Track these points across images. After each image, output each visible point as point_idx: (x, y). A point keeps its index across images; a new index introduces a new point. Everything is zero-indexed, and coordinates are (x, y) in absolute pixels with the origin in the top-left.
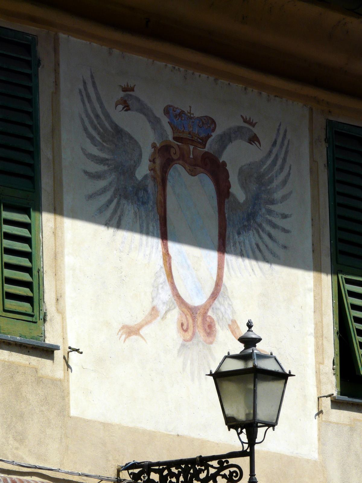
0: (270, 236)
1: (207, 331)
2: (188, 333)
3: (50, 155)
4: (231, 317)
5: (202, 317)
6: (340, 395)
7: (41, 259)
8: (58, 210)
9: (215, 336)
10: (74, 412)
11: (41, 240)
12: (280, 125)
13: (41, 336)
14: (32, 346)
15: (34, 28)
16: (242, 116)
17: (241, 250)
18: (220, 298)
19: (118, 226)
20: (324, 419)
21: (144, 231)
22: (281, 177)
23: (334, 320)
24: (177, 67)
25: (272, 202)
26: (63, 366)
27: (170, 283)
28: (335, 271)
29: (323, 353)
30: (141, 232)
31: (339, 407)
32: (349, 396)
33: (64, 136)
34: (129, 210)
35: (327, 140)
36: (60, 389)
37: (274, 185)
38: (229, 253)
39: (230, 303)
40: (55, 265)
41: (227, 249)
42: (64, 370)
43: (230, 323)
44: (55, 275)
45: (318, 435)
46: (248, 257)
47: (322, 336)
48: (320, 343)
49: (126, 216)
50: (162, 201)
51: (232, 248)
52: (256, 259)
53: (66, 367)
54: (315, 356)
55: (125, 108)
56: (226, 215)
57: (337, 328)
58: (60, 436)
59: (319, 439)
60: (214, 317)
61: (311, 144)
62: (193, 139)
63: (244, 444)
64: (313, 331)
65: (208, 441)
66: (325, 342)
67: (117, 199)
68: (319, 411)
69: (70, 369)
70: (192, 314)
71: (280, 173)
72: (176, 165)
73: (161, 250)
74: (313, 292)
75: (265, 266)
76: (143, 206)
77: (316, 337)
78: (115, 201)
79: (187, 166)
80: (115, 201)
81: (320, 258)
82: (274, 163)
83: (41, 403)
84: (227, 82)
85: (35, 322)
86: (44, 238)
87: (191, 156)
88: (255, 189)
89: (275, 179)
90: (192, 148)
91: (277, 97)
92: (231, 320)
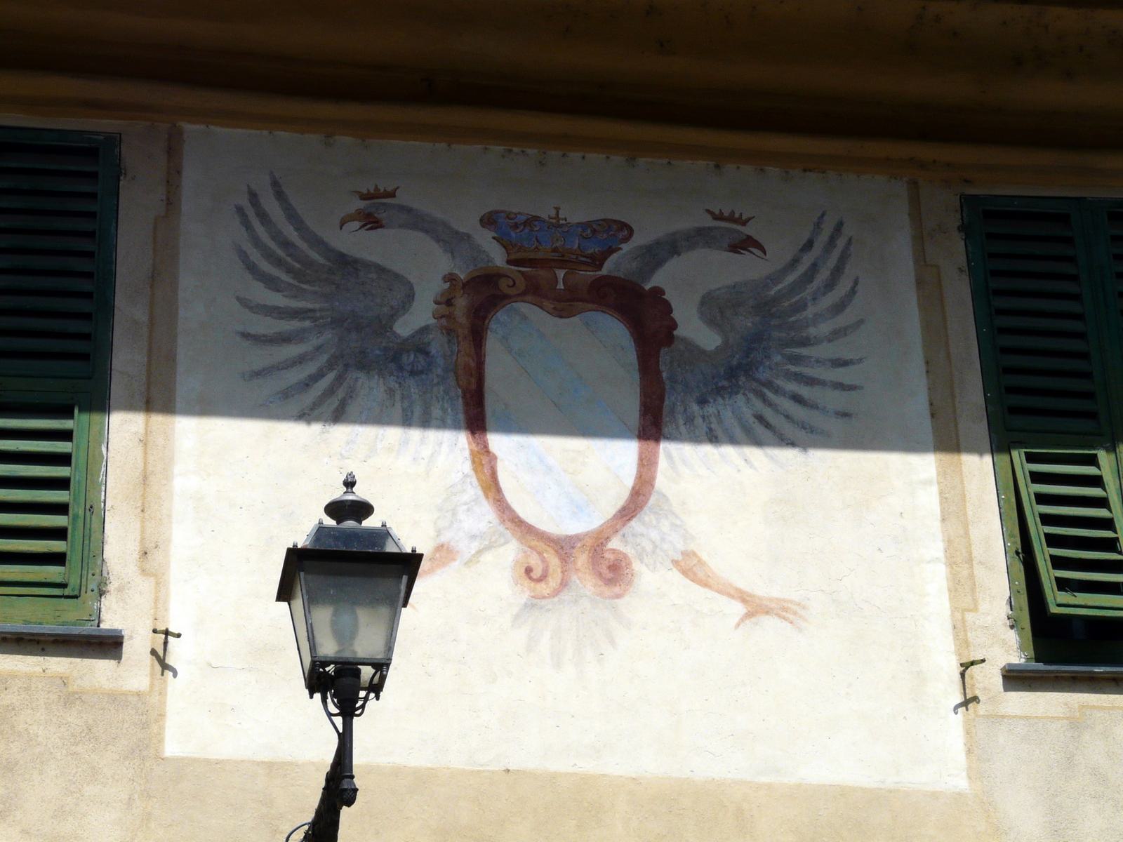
0: (797, 399)
1: (604, 576)
2: (547, 584)
3: (141, 315)
4: (680, 546)
5: (589, 553)
6: (1036, 662)
7: (1095, 672)
8: (158, 398)
9: (630, 583)
10: (173, 747)
11: (105, 456)
12: (823, 215)
13: (90, 620)
14: (52, 639)
15: (108, 121)
16: (708, 211)
17: (711, 430)
18: (646, 516)
19: (339, 416)
20: (982, 712)
21: (416, 416)
22: (828, 300)
23: (1004, 529)
24: (515, 149)
25: (805, 342)
26: (149, 668)
27: (491, 500)
28: (1000, 444)
29: (973, 590)
30: (407, 421)
31: (1030, 686)
32: (1046, 663)
33: (187, 282)
34: (372, 387)
35: (963, 228)
36: (146, 715)
37: (810, 312)
38: (670, 438)
39: (678, 522)
40: (143, 495)
41: (665, 430)
42: (152, 675)
43: (680, 558)
44: (142, 511)
45: (965, 745)
46: (733, 441)
47: (970, 560)
48: (965, 573)
49: (363, 398)
50: (473, 364)
51: (683, 429)
52: (758, 442)
53: (158, 668)
54: (950, 599)
55: (369, 226)
56: (664, 375)
57: (1014, 543)
58: (127, 797)
59: (969, 752)
60: (629, 551)
61: (919, 240)
62: (565, 258)
63: (332, 717)
64: (941, 554)
65: (604, 775)
66: (979, 571)
67: (335, 372)
68: (968, 698)
69: (172, 671)
70: (560, 551)
71: (824, 294)
72: (513, 304)
73: (466, 446)
74: (937, 486)
75: (789, 455)
76: (414, 378)
77: (951, 563)
78: (331, 376)
79: (546, 304)
80: (331, 376)
81: (956, 426)
82: (809, 276)
83: (72, 740)
84: (665, 161)
85: (76, 597)
86: (112, 451)
87: (561, 286)
88: (749, 324)
89: (809, 304)
90: (561, 274)
91: (810, 171)
92: (680, 553)
